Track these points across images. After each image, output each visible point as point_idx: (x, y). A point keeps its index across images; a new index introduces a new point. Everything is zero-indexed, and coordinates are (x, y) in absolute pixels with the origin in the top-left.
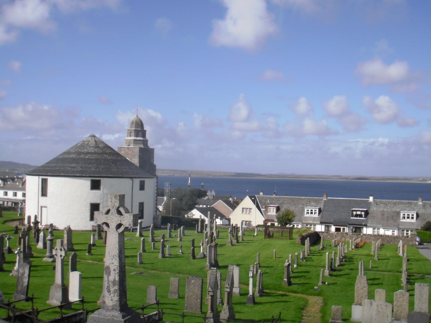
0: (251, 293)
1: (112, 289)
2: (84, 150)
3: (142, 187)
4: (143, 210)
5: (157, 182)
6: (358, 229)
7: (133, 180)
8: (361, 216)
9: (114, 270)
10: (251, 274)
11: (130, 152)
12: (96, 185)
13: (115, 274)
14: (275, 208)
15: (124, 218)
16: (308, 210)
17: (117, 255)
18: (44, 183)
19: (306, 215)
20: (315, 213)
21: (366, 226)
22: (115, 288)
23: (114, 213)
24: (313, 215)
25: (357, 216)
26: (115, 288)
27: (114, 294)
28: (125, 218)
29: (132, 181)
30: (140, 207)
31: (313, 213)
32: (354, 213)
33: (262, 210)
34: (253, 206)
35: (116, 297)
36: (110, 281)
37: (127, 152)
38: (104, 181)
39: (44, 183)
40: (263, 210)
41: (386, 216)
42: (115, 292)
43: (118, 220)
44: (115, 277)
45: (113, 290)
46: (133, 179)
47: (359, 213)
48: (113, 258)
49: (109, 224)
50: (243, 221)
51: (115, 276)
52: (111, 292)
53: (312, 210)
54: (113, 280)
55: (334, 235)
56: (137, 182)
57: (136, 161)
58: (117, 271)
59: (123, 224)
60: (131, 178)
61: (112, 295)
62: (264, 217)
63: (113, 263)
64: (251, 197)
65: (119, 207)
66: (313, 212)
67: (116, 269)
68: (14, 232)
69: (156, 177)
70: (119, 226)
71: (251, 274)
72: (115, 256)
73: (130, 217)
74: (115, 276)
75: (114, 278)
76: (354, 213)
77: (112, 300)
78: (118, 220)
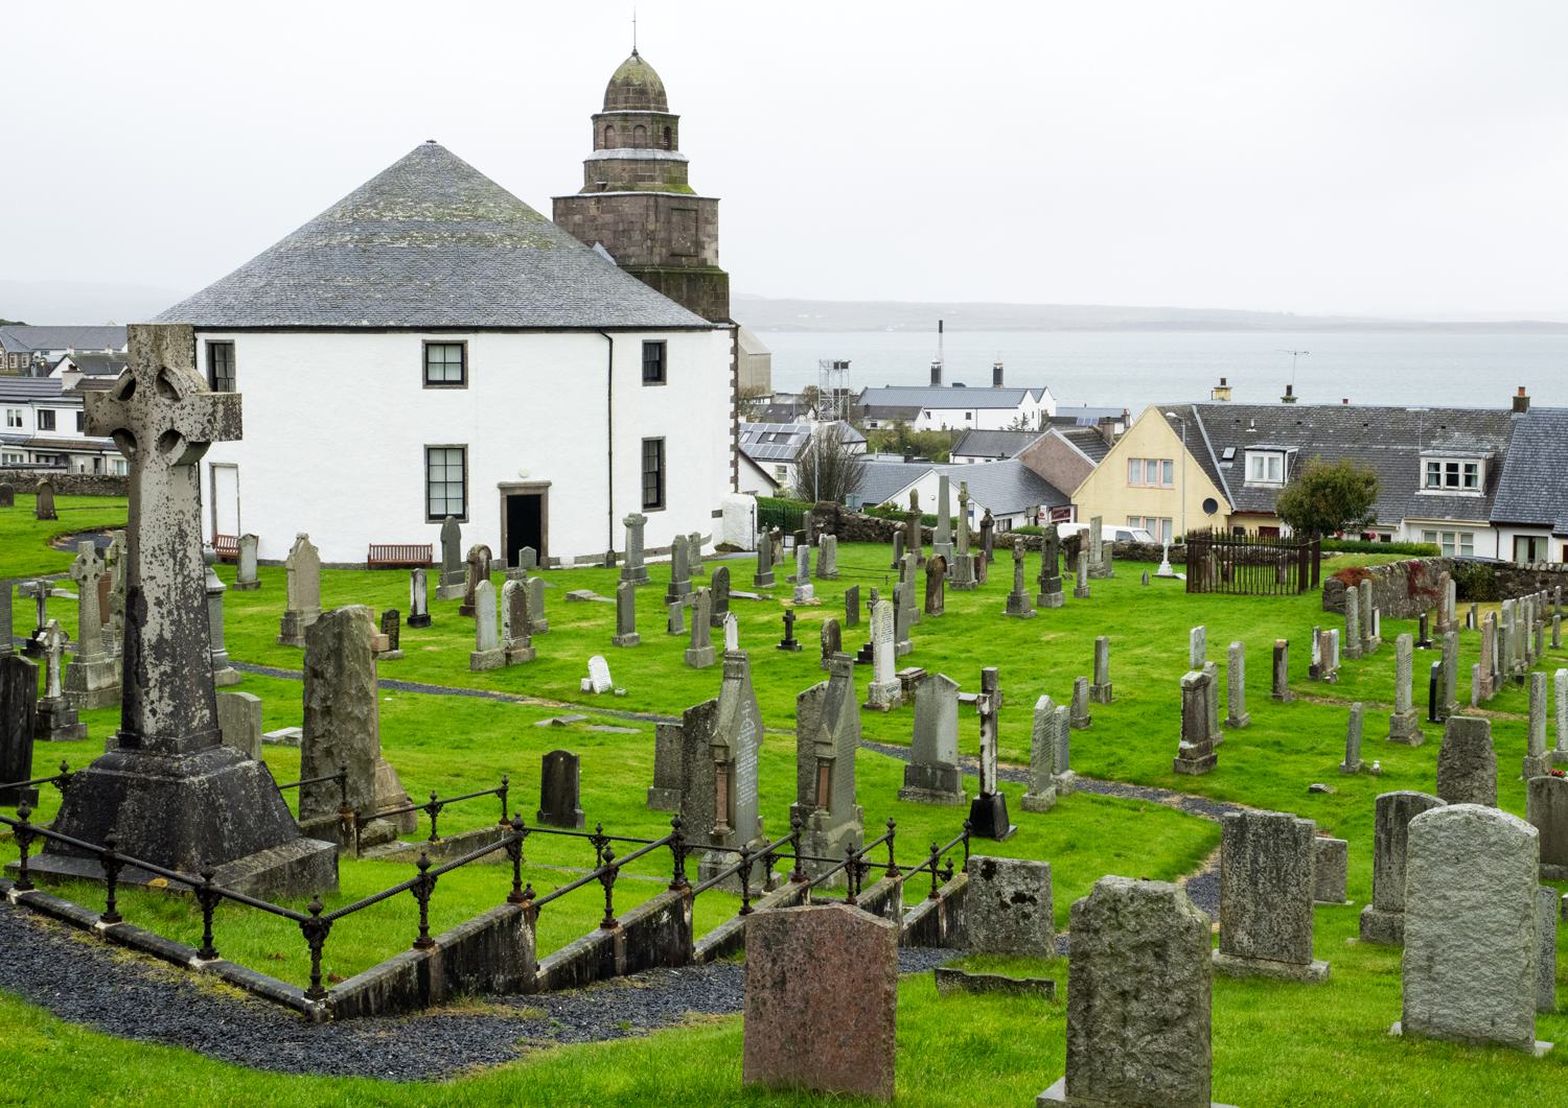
2: (392, 210)
3: (655, 369)
4: (664, 469)
5: (735, 350)
7: (611, 340)
11: (609, 218)
13: (162, 617)
14: (1280, 455)
15: (183, 408)
16: (1437, 466)
20: (1469, 481)
22: (162, 668)
23: (148, 393)
24: (1461, 491)
26: (162, 668)
27: (161, 690)
28: (186, 411)
29: (608, 342)
30: (646, 458)
31: (1462, 480)
36: (146, 644)
37: (594, 219)
40: (1225, 470)
43: (164, 418)
44: (162, 630)
45: (157, 676)
46: (610, 335)
48: (153, 560)
49: (136, 436)
50: (429, 383)
51: (162, 625)
52: (151, 684)
53: (1452, 467)
54: (154, 639)
55: (1539, 577)
56: (630, 349)
59: (182, 431)
60: (602, 330)
62: (1228, 500)
66: (1461, 472)
68: (885, 870)
69: (726, 325)
72: (158, 552)
73: (203, 404)
74: (162, 625)
75: (158, 632)
78: (164, 418)
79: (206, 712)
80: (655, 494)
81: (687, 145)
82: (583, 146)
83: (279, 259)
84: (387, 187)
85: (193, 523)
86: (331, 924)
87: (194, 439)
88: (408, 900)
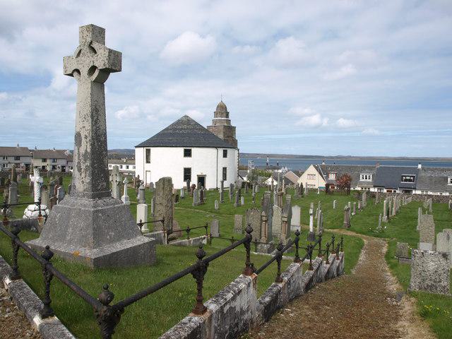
0: (311, 230)
1: (83, 167)
3: (225, 155)
6: (407, 191)
8: (410, 180)
9: (86, 137)
10: (311, 212)
12: (188, 154)
17: (89, 114)
18: (148, 152)
19: (361, 180)
21: (415, 189)
24: (368, 180)
25: (406, 180)
30: (223, 171)
32: (404, 178)
33: (324, 176)
34: (317, 173)
35: (87, 177)
38: (194, 150)
39: (148, 152)
41: (434, 180)
42: (86, 170)
47: (407, 178)
52: (83, 170)
57: (221, 136)
58: (89, 138)
60: (216, 148)
61: (83, 175)
63: (84, 127)
64: (314, 166)
65: (91, 43)
67: (87, 135)
70: (93, 69)
71: (311, 212)
76: (404, 178)
77: (83, 182)
79: (105, 184)
80: (225, 177)
81: (230, 117)
82: (212, 117)
83: (158, 135)
84: (179, 122)
85: (101, 107)
86: (122, 311)
87: (101, 68)
88: (190, 281)
